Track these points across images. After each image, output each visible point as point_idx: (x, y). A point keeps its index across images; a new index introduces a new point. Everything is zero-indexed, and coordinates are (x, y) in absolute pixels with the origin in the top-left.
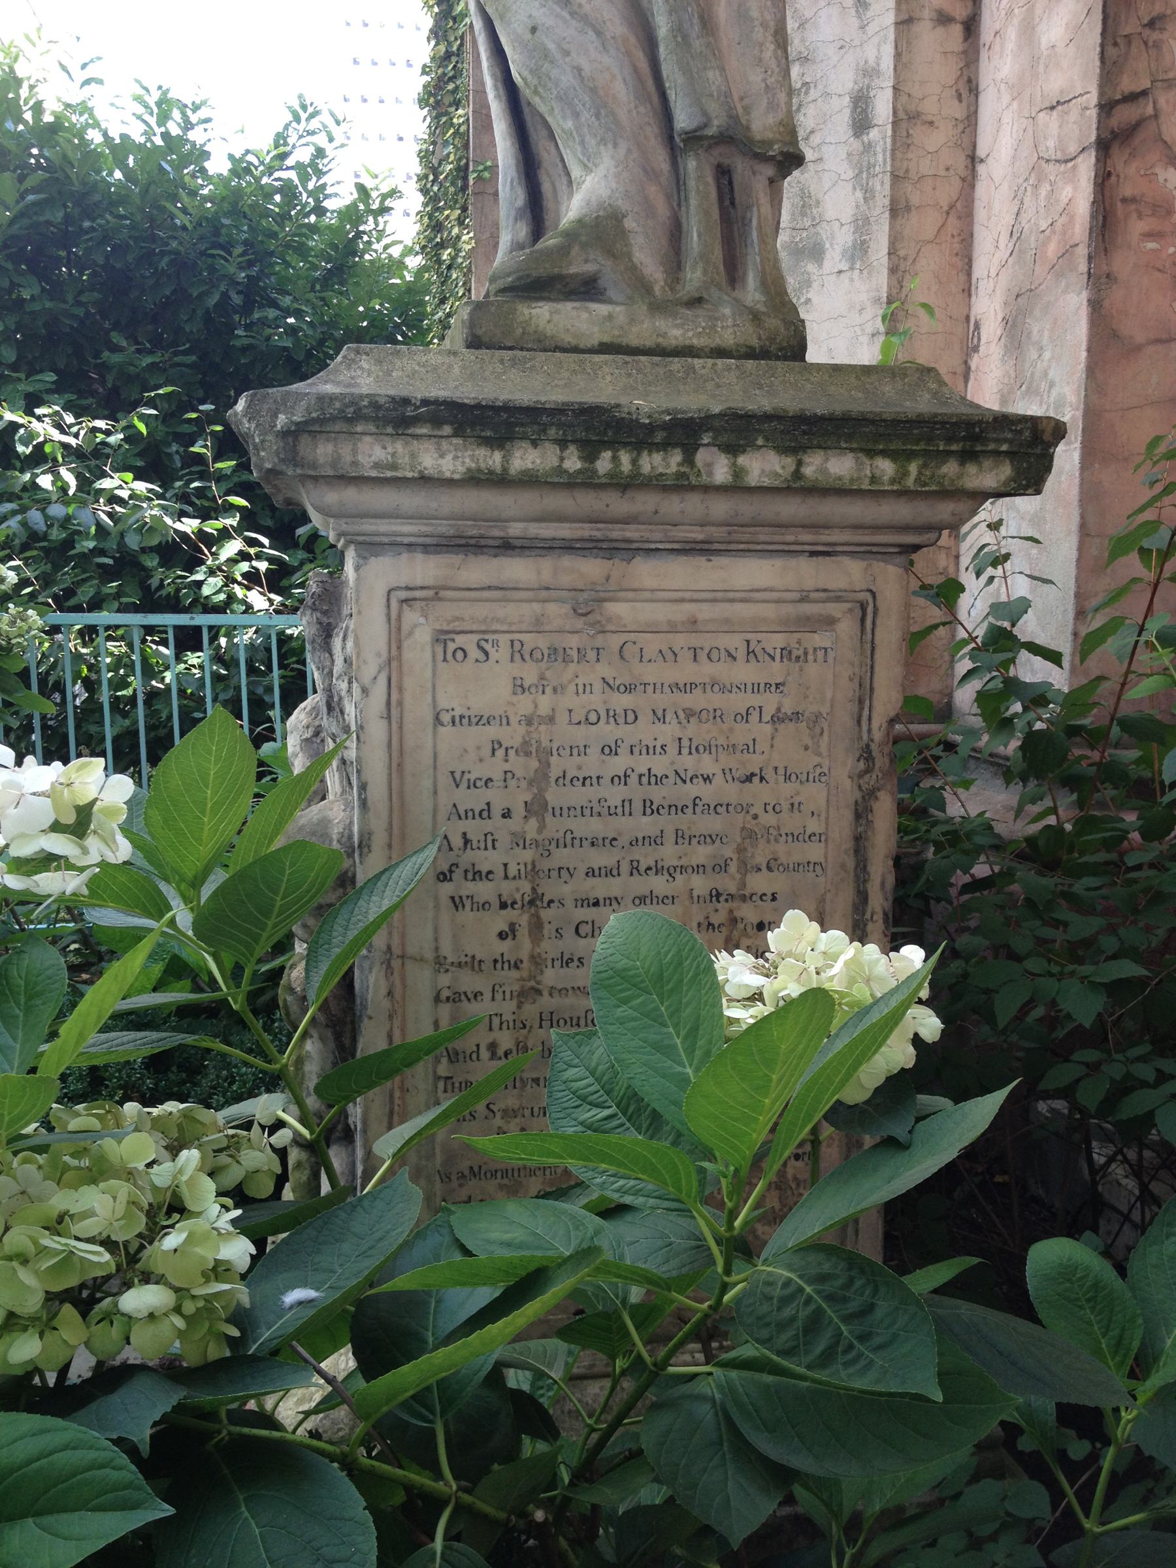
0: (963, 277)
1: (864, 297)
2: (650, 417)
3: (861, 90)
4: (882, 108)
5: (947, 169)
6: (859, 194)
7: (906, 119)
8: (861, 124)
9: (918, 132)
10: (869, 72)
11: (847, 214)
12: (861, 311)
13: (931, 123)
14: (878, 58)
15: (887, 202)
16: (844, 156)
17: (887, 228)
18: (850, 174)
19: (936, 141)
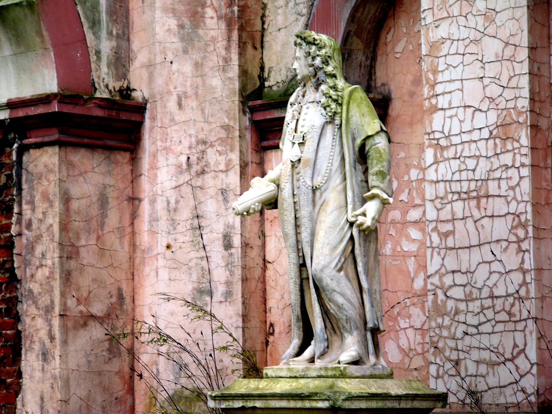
0: (263, 306)
1: (232, 313)
2: (273, 342)
3: (227, 233)
4: (237, 241)
5: (257, 264)
6: (228, 272)
7: (245, 245)
8: (228, 246)
9: (248, 250)
10: (229, 226)
11: (223, 279)
12: (231, 318)
13: (252, 247)
14: (234, 222)
15: (240, 277)
16: (221, 257)
17: (240, 287)
18: (224, 264)
19: (254, 253)
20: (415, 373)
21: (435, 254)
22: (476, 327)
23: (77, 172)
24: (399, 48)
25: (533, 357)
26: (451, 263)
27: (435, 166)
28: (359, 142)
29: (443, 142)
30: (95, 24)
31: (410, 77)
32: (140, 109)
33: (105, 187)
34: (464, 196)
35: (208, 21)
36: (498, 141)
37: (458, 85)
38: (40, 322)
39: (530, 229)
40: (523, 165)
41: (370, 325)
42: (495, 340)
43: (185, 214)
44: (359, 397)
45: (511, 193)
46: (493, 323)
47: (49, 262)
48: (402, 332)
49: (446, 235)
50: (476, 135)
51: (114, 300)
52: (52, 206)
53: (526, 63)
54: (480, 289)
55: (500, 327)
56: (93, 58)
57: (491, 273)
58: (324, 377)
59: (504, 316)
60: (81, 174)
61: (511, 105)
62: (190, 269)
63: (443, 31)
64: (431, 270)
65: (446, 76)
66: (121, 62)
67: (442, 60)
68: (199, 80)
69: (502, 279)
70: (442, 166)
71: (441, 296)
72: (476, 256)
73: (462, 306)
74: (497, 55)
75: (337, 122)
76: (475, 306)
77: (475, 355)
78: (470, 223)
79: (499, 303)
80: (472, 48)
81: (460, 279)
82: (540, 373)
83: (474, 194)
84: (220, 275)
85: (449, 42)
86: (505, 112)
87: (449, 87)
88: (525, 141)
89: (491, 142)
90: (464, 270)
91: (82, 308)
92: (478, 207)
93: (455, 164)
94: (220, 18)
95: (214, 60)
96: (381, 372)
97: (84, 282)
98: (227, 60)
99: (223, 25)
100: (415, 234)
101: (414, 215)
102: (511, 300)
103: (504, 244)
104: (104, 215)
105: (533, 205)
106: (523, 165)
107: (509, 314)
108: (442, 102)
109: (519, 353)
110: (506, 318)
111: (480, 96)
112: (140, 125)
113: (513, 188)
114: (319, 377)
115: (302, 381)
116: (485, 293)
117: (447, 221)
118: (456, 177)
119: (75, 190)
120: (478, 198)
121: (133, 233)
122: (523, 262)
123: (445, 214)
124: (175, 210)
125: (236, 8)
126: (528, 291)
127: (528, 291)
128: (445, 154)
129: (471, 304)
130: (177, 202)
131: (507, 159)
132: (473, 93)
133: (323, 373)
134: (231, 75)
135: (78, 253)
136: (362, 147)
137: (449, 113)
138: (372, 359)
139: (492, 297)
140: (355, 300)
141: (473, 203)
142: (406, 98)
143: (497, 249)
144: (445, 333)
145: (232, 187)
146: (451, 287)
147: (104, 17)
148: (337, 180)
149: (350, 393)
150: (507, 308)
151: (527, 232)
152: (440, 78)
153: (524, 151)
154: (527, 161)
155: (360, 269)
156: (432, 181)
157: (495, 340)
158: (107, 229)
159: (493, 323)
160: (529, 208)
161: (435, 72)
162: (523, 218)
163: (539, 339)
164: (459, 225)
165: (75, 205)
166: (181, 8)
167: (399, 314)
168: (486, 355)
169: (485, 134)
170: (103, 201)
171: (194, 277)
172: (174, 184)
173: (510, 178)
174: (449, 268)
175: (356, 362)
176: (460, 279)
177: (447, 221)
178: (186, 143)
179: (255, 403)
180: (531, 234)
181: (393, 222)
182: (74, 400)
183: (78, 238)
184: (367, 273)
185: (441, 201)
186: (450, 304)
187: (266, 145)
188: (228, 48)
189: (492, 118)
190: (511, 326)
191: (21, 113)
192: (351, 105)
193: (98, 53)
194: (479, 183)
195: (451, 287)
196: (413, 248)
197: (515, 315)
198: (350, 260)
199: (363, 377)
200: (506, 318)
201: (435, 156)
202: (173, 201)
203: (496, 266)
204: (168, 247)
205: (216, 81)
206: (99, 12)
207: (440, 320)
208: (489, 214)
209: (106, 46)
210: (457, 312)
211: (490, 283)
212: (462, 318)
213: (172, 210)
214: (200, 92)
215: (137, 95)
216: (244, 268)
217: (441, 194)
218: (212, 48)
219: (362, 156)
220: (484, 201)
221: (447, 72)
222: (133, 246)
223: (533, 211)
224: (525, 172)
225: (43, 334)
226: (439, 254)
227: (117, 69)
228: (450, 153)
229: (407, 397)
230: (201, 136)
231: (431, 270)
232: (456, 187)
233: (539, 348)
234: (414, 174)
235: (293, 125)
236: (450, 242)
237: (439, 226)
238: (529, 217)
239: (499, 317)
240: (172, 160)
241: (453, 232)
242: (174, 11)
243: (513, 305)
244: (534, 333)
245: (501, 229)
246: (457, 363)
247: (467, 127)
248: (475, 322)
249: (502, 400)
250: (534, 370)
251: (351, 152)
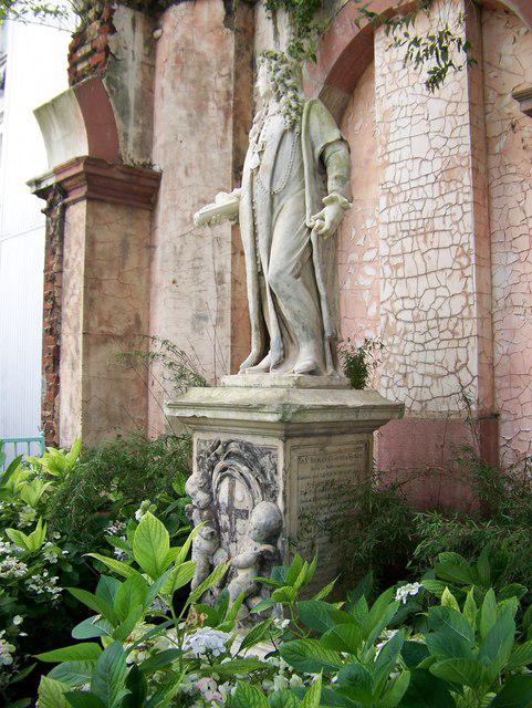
4: (228, 278)
8: (220, 282)
21: (387, 283)
22: (423, 345)
23: (102, 222)
25: (475, 371)
26: (401, 291)
27: (387, 211)
28: (318, 150)
29: (394, 190)
30: (124, 113)
31: (366, 148)
32: (157, 177)
33: (126, 235)
34: (412, 233)
35: (210, 111)
36: (443, 184)
37: (407, 142)
38: (71, 338)
39: (473, 257)
40: (465, 202)
41: (328, 334)
42: (439, 355)
43: (188, 256)
44: (313, 409)
45: (455, 227)
46: (438, 340)
47: (78, 292)
49: (397, 267)
50: (423, 181)
51: (132, 323)
52: (80, 247)
53: (467, 116)
54: (426, 312)
55: (444, 344)
56: (121, 139)
57: (436, 298)
58: (277, 387)
59: (448, 335)
60: (106, 224)
61: (453, 152)
62: (191, 299)
63: (395, 99)
64: (383, 297)
65: (397, 137)
66: (145, 143)
67: (393, 124)
68: (202, 155)
69: (447, 302)
70: (393, 210)
71: (392, 319)
72: (423, 282)
73: (410, 327)
74: (441, 113)
75: (297, 130)
76: (422, 326)
77: (421, 369)
78: (418, 256)
79: (443, 324)
80: (419, 110)
81: (409, 304)
82: (480, 385)
83: (422, 231)
84: (213, 304)
85: (399, 109)
86: (448, 159)
87: (399, 145)
88: (467, 180)
89: (436, 185)
90: (412, 295)
91: (103, 328)
92: (425, 241)
93: (405, 207)
94: (219, 109)
95: (213, 140)
96: (338, 383)
97: (106, 307)
98: (224, 140)
99: (222, 115)
101: (369, 256)
102: (454, 320)
103: (449, 272)
104: (124, 258)
105: (476, 236)
106: (465, 202)
107: (453, 332)
108: (393, 157)
109: (462, 367)
110: (450, 336)
111: (427, 146)
112: (156, 189)
113: (457, 223)
114: (273, 386)
115: (253, 391)
116: (431, 315)
117: (398, 255)
118: (406, 217)
119: (100, 236)
120: (425, 234)
121: (150, 273)
122: (466, 286)
123: (397, 249)
124: (181, 253)
125: (232, 102)
126: (470, 312)
127: (470, 312)
128: (396, 200)
129: (417, 325)
130: (182, 247)
131: (451, 198)
132: (421, 147)
133: (276, 383)
134: (226, 150)
135: (100, 285)
136: (322, 157)
137: (398, 166)
138: (330, 370)
139: (437, 318)
140: (312, 307)
141: (421, 238)
142: (363, 164)
143: (442, 276)
144: (395, 351)
145: (225, 236)
146: (401, 311)
147: (132, 109)
148: (295, 187)
149: (302, 406)
150: (451, 328)
151: (470, 260)
152: (391, 138)
153: (468, 189)
154: (470, 198)
155: (318, 276)
156: (384, 223)
157: (439, 355)
158: (127, 268)
159: (438, 340)
160: (472, 239)
161: (387, 134)
162: (466, 249)
163: (479, 354)
164: (408, 258)
165: (99, 247)
166: (190, 101)
168: (430, 369)
169: (431, 179)
170: (125, 246)
171: (194, 307)
172: (180, 232)
173: (455, 214)
174: (399, 295)
175: (312, 372)
176: (409, 304)
177: (398, 255)
178: (190, 202)
179: (511, 376)
180: (473, 262)
181: (352, 263)
182: (94, 400)
183: (102, 274)
184: (325, 281)
185: (392, 239)
186: (400, 326)
187: (329, 415)
188: (225, 131)
189: (438, 164)
190: (454, 343)
191: (62, 177)
192: (311, 114)
193: (126, 135)
194: (426, 221)
195: (401, 311)
196: (368, 282)
197: (458, 334)
198: (308, 266)
199: (319, 387)
200: (450, 336)
201: (388, 201)
202: (179, 247)
203: (442, 291)
204: (174, 282)
205: (215, 156)
206: (128, 106)
207: (390, 340)
208: (435, 246)
209: (133, 131)
210: (405, 333)
211: (436, 306)
212: (410, 337)
213: (178, 254)
214: (203, 163)
215: (156, 169)
216: (233, 299)
217: (393, 232)
218: (212, 131)
219: (321, 166)
220: (430, 236)
221: (398, 133)
222: (149, 282)
223: (475, 241)
224: (468, 208)
225: (72, 348)
226: (391, 283)
227: (141, 149)
228: (401, 198)
229: (364, 408)
230: (202, 196)
231: (383, 297)
232: (405, 226)
233: (480, 362)
234: (369, 223)
235: (255, 139)
236: (400, 274)
237: (391, 259)
238: (472, 246)
239: (443, 336)
240: (179, 214)
241: (403, 264)
242: (185, 105)
243: (456, 325)
244: (476, 350)
245: (446, 258)
246: (405, 376)
247: (415, 175)
248: (422, 340)
249: (445, 408)
250: (475, 382)
251: (311, 159)
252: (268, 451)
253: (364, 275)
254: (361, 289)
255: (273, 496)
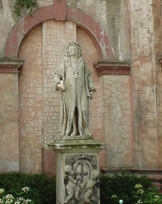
20: (31, 139)
24: (27, 50)
48: (27, 128)
100: (31, 101)
101: (31, 96)
167: (26, 123)
181: (24, 98)
252: (92, 157)
253: (29, 102)
254: (28, 107)
255: (96, 168)
